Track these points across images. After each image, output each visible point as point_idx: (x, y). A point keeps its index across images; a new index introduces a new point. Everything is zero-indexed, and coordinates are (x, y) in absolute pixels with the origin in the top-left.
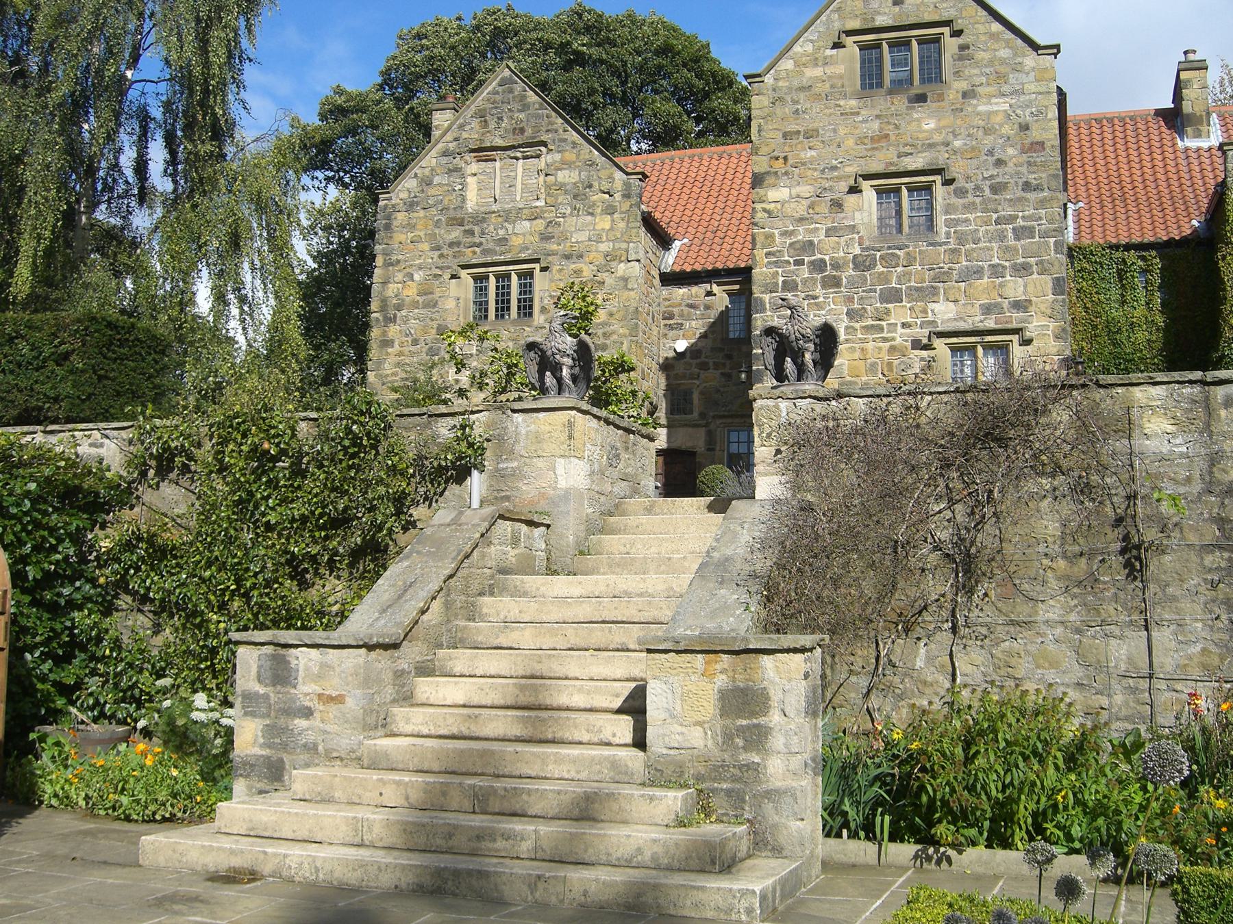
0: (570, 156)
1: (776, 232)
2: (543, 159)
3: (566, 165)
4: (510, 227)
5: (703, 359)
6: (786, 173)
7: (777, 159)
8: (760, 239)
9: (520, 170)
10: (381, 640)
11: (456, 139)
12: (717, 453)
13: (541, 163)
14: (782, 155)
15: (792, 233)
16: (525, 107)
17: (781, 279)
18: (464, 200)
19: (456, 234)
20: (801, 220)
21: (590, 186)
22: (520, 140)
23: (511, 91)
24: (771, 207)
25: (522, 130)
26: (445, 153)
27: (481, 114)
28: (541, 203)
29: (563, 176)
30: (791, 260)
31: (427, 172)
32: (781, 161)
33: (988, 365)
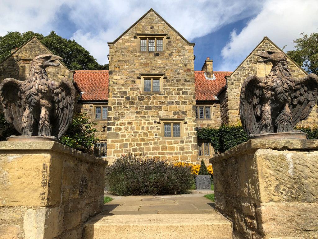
1: (116, 88)
17: (117, 101)
30: (120, 96)
32: (118, 68)
33: (56, 108)
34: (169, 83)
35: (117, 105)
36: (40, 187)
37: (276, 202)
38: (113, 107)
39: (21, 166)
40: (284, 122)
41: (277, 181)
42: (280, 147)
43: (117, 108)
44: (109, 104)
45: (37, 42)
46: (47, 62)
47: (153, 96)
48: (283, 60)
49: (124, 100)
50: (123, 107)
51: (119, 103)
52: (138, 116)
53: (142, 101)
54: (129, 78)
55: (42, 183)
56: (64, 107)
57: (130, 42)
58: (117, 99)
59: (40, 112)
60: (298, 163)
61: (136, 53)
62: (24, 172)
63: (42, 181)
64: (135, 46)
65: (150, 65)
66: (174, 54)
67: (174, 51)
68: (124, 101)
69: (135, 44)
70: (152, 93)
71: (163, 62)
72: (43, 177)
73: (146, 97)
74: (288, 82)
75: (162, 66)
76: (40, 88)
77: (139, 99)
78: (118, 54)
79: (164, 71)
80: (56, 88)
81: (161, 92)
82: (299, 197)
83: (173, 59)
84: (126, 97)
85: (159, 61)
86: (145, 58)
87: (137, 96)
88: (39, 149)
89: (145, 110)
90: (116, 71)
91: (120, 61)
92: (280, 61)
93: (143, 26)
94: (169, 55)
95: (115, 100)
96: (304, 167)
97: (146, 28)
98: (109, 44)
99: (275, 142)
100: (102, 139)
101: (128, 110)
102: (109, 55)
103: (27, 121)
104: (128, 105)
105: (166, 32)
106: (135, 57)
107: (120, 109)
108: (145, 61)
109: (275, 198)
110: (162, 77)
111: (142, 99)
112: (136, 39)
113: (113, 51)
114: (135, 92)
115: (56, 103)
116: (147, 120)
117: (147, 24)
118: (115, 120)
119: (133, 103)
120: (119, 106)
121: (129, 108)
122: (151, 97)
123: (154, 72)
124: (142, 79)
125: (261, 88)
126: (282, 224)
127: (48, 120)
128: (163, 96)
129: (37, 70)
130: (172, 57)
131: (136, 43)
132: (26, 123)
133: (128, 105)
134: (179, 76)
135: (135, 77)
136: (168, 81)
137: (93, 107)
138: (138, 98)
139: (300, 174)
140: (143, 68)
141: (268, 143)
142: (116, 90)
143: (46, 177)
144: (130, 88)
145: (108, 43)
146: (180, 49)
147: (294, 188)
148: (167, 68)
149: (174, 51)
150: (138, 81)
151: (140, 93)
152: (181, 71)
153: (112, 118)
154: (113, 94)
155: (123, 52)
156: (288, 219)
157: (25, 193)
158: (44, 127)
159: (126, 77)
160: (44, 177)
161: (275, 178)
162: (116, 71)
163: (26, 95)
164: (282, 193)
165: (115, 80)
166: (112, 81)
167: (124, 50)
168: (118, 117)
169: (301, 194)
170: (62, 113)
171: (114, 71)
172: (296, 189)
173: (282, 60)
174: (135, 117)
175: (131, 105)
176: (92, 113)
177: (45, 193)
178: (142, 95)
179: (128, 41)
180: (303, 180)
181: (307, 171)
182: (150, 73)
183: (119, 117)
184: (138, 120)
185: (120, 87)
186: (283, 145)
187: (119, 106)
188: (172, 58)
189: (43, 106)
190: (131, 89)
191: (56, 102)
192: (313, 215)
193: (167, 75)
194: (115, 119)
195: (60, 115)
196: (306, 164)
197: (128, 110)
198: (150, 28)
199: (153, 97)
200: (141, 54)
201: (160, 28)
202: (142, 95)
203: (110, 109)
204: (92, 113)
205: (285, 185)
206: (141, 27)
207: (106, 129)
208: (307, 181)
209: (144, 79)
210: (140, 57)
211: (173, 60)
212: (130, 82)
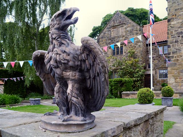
0: (129, 25)
1: (173, 31)
2: (124, 27)
3: (129, 27)
4: (119, 39)
5: (154, 58)
6: (176, 18)
7: (174, 15)
8: (169, 33)
9: (120, 29)
10: (162, 52)
11: (109, 25)
12: (157, 74)
13: (124, 27)
14: (175, 14)
15: (177, 30)
16: (121, 18)
17: (174, 40)
18: (111, 35)
19: (110, 41)
20: (180, 27)
21: (133, 30)
22: (120, 24)
23: (118, 16)
24: (172, 26)
25: (121, 22)
26: (107, 28)
27: (114, 21)
28: (124, 34)
29: (128, 29)
30: (177, 36)
31: (104, 32)
32: (175, 16)
33: (88, 78)
35: (175, 43)
38: (171, 45)
43: (174, 45)
44: (169, 44)
45: (119, 14)
46: (63, 22)
50: (180, 43)
56: (95, 76)
76: (58, 59)
78: (174, 5)
80: (80, 53)
95: (173, 39)
102: (167, 8)
103: (59, 96)
107: (177, 45)
113: (171, 3)
115: (86, 72)
129: (55, 35)
132: (57, 98)
142: (174, 32)
153: (171, 53)
155: (179, 2)
158: (73, 105)
162: (173, 18)
166: (171, 27)
183: (177, 51)
185: (177, 29)
194: (173, 53)
195: (94, 84)
203: (169, 47)
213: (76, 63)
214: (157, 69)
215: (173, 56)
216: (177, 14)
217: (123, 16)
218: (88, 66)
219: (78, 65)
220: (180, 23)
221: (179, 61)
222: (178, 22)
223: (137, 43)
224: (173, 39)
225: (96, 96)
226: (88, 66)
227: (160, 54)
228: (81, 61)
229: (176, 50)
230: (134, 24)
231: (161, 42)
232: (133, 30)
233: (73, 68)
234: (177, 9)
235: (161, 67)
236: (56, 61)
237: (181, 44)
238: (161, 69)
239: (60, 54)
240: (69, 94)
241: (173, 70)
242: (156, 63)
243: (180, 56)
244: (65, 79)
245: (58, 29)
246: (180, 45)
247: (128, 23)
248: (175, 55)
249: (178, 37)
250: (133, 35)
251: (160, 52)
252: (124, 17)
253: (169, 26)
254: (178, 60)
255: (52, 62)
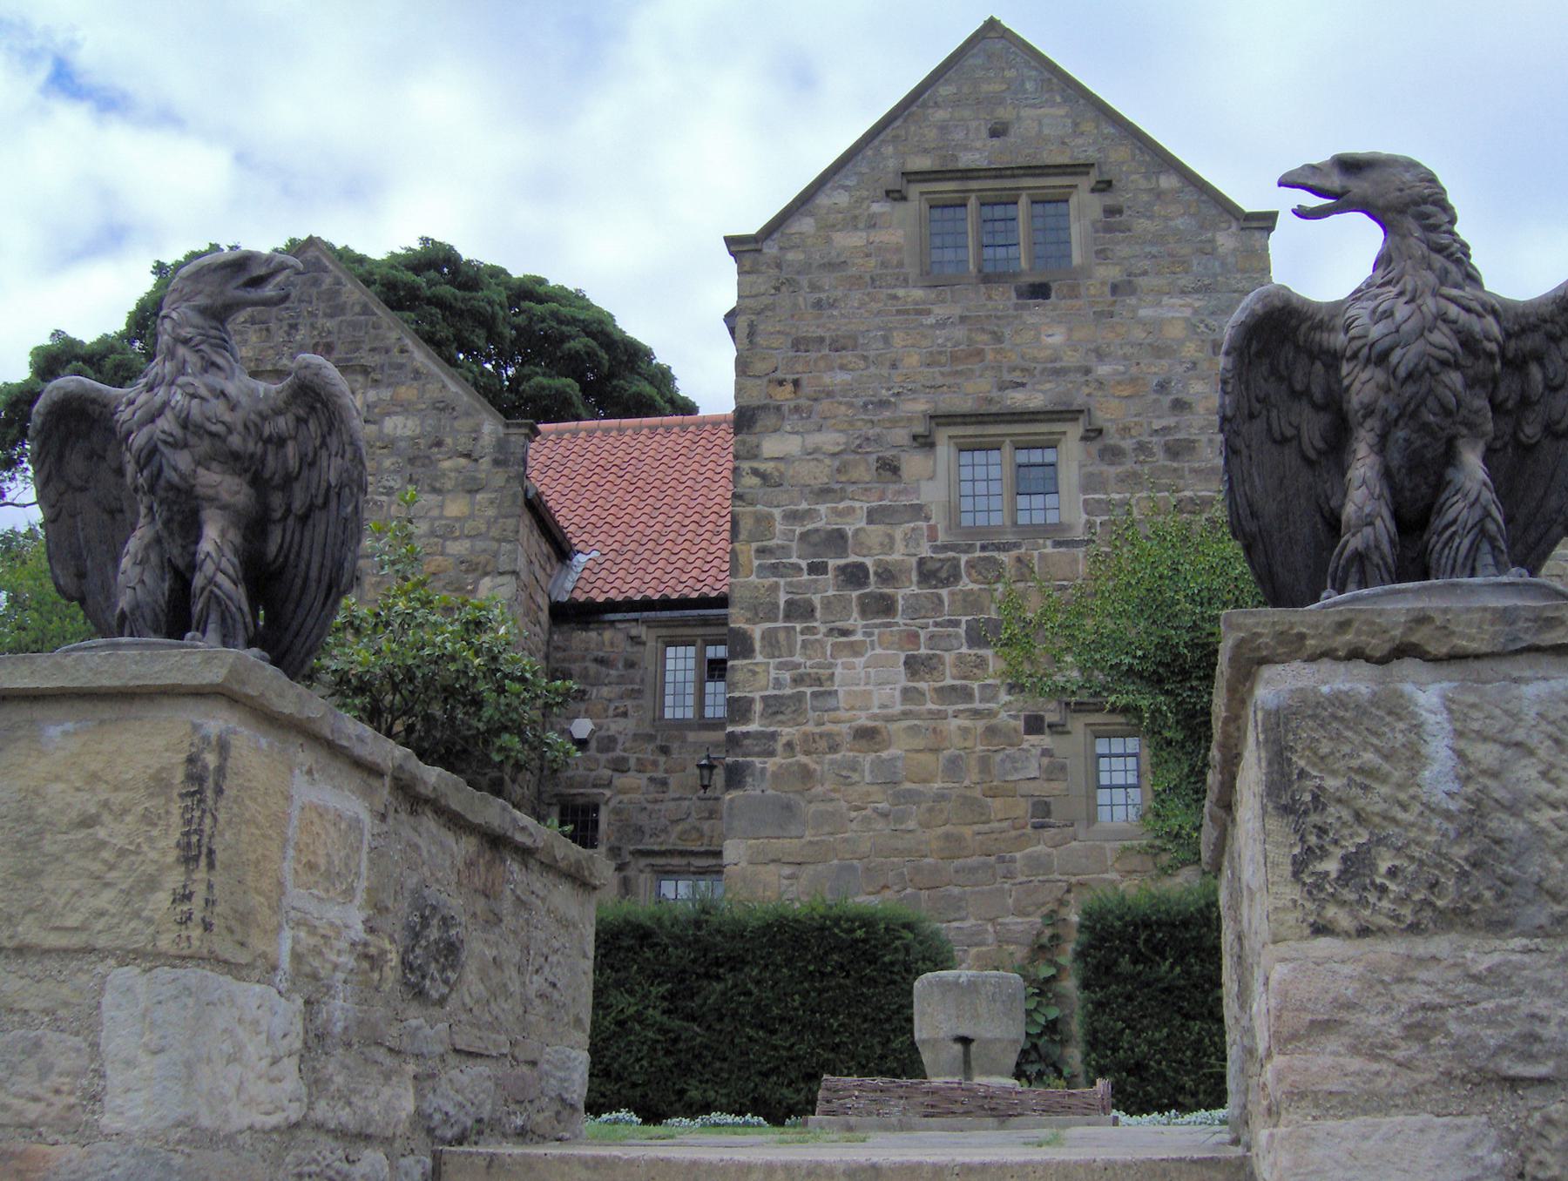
3: (405, 408)
5: (618, 753)
6: (797, 409)
7: (781, 383)
8: (746, 525)
14: (790, 377)
15: (809, 514)
16: (337, 310)
17: (782, 598)
21: (439, 444)
23: (316, 283)
32: (789, 387)
33: (278, 515)
34: (1120, 469)
35: (787, 617)
36: (170, 868)
37: (1348, 935)
38: (757, 631)
39: (95, 766)
40: (1457, 540)
41: (1360, 830)
42: (1378, 646)
43: (782, 636)
45: (325, 270)
47: (1015, 553)
48: (1425, 201)
49: (827, 588)
50: (823, 629)
51: (799, 610)
52: (922, 685)
53: (944, 592)
54: (860, 446)
55: (178, 845)
57: (861, 226)
58: (782, 582)
59: (197, 539)
60: (1478, 732)
61: (901, 292)
62: (103, 797)
63: (178, 835)
64: (898, 249)
65: (990, 356)
66: (1142, 281)
67: (1146, 264)
68: (830, 593)
69: (892, 236)
70: (1011, 539)
71: (1076, 336)
72: (183, 815)
73: (971, 565)
74: (1453, 311)
75: (1071, 359)
77: (927, 574)
79: (1086, 390)
81: (1070, 527)
82: (1476, 907)
83: (1142, 313)
84: (842, 570)
85: (1050, 333)
86: (963, 319)
87: (914, 561)
88: (166, 686)
89: (964, 650)
90: (778, 408)
91: (798, 344)
92: (1407, 205)
93: (943, 128)
94: (1115, 289)
95: (774, 588)
96: (1509, 752)
97: (958, 136)
98: (736, 245)
99: (1356, 625)
100: (703, 849)
101: (857, 654)
104: (855, 621)
105: (1091, 154)
106: (899, 312)
107: (805, 644)
108: (960, 333)
109: (1344, 920)
110: (1074, 431)
111: (947, 579)
112: (900, 206)
113: (762, 283)
114: (899, 533)
116: (976, 713)
117: (967, 113)
118: (776, 713)
119: (885, 606)
120: (798, 627)
121: (858, 637)
122: (1001, 564)
123: (1018, 399)
124: (944, 450)
125: (1333, 359)
126: (1376, 1050)
127: (231, 571)
128: (1080, 552)
130: (1133, 301)
131: (900, 232)
133: (855, 615)
134: (1187, 417)
135: (901, 435)
136: (1112, 454)
137: (644, 644)
138: (921, 573)
139: (1483, 790)
140: (950, 381)
141: (1316, 626)
142: (779, 526)
143: (196, 820)
144: (866, 505)
145: (731, 241)
146: (1186, 250)
147: (1451, 861)
148: (1103, 370)
149: (1146, 264)
150: (914, 464)
151: (932, 536)
152: (1197, 387)
154: (761, 552)
156: (1407, 1021)
157: (109, 894)
158: (214, 606)
159: (842, 438)
160: (189, 822)
161: (1346, 814)
162: (778, 408)
163: (135, 447)
164: (1383, 890)
165: (772, 464)
166: (755, 472)
167: (827, 280)
168: (790, 697)
169: (1488, 894)
170: (307, 534)
171: (764, 408)
172: (1460, 866)
173: (1417, 204)
174: (897, 693)
175: (877, 614)
176: (642, 681)
177: (191, 894)
178: (945, 548)
179: (852, 223)
180: (1501, 823)
181: (1526, 773)
182: (994, 409)
183: (799, 697)
184: (918, 716)
185: (804, 506)
186: (1393, 639)
187: (798, 627)
188: (1134, 309)
189: (211, 500)
190: (872, 516)
191: (274, 483)
192: (1541, 1005)
193: (1101, 417)
196: (1519, 734)
197: (855, 648)
198: (984, 133)
199: (1019, 560)
200: (932, 294)
201: (1042, 131)
202: (945, 548)
204: (642, 681)
205: (1399, 849)
206: (932, 134)
207: (719, 777)
208: (1521, 827)
209: (953, 450)
210: (929, 312)
211: (1142, 322)
212: (863, 471)
213: (251, 446)
214: (643, 862)
215: (773, 736)
216: (804, 382)
217: (353, 293)
218: (291, 462)
219: (252, 456)
220: (828, 461)
221: (818, 789)
222: (810, 445)
223: (470, 578)
224: (777, 585)
225: (292, 607)
226: (293, 464)
227: (668, 714)
228: (268, 440)
229: (797, 681)
230: (453, 388)
231: (684, 603)
232: (439, 444)
233: (234, 461)
234: (807, 340)
235: (672, 841)
236: (185, 423)
237: (831, 631)
238: (676, 861)
239: (202, 398)
240: (208, 554)
241: (772, 867)
242: (636, 796)
243: (823, 744)
244: (197, 498)
245: (203, 311)
246: (831, 640)
247: (401, 367)
248: (788, 732)
249: (815, 569)
250: (434, 490)
251: (669, 700)
252: (366, 310)
253: (746, 466)
254: (806, 774)
255: (166, 423)
